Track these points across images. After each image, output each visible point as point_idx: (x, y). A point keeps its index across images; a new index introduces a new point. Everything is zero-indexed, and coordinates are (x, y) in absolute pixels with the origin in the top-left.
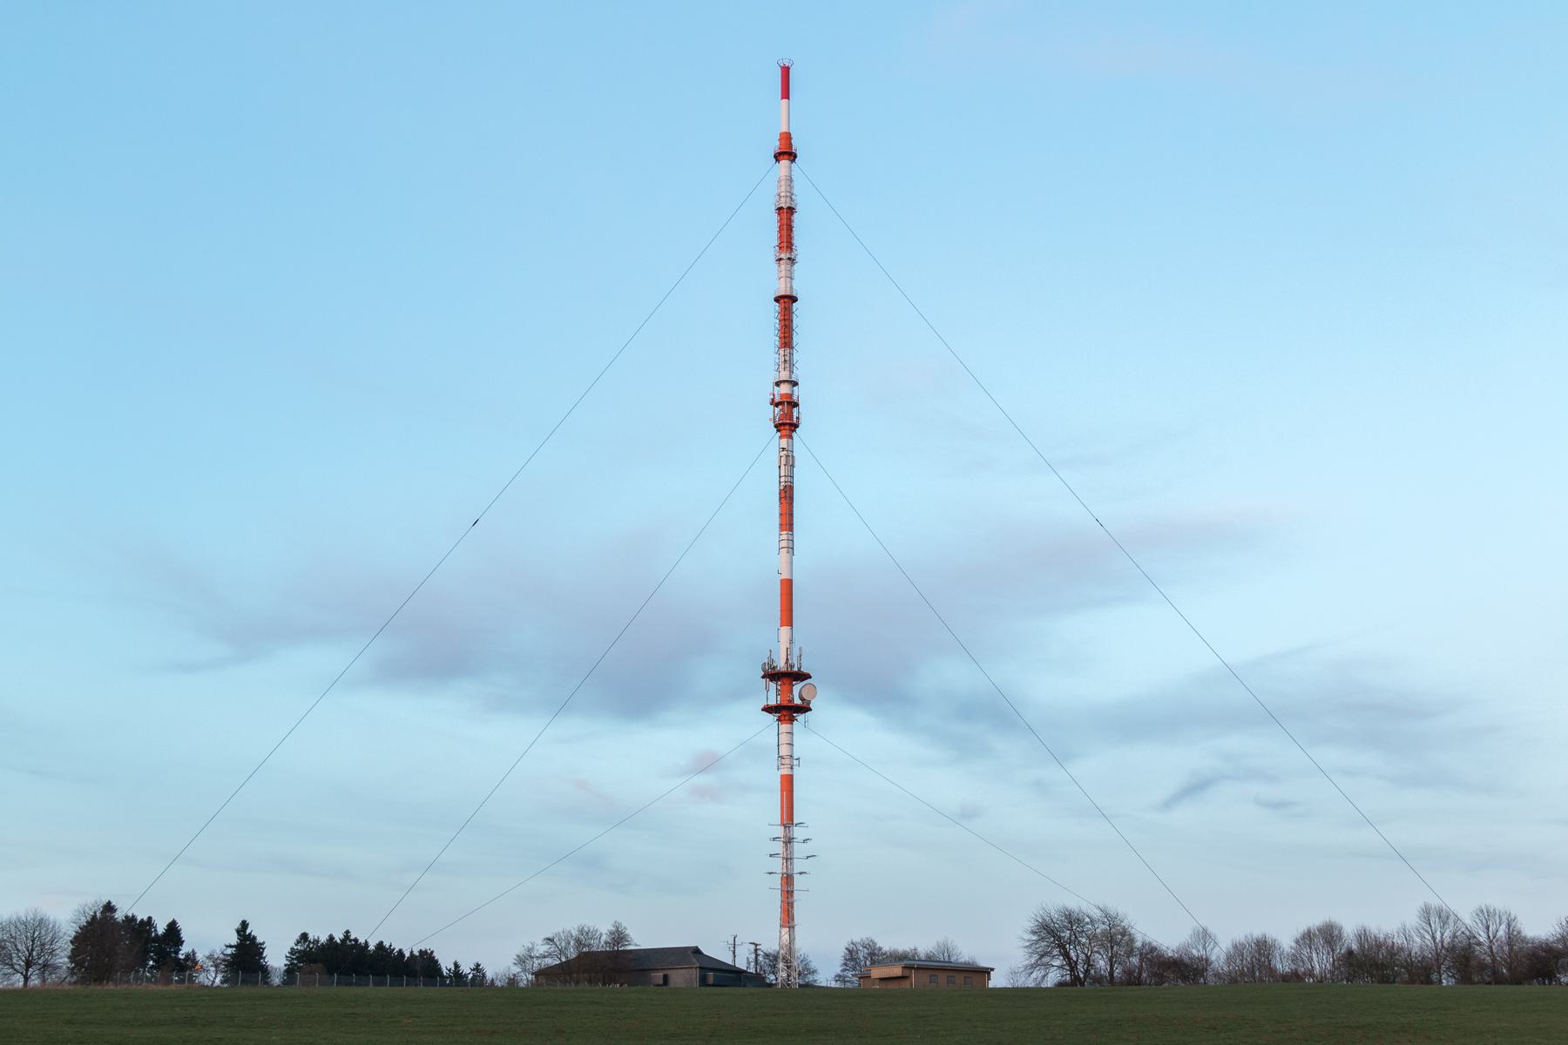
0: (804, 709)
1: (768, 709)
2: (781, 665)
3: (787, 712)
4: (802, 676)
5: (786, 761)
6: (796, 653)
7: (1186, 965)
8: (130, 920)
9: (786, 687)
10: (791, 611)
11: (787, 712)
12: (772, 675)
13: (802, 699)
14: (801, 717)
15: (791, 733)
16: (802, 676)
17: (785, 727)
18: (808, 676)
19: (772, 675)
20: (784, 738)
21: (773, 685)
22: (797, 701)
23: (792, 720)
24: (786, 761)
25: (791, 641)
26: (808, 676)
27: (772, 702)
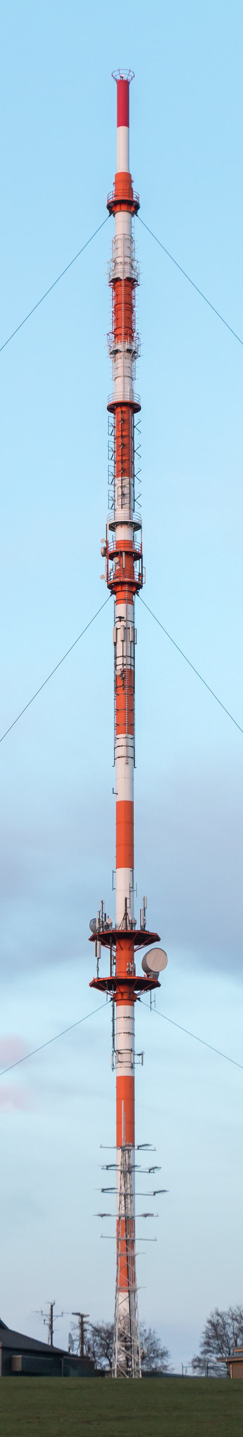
0: (150, 983)
1: (99, 984)
2: (117, 922)
4: (146, 938)
5: (125, 1057)
6: (138, 906)
9: (124, 953)
11: (125, 988)
12: (105, 937)
13: (147, 970)
14: (145, 996)
15: (131, 1018)
16: (146, 938)
17: (122, 1010)
19: (105, 937)
20: (121, 1025)
22: (140, 973)
23: (132, 1000)
24: (125, 1057)
25: (131, 889)
27: (105, 974)
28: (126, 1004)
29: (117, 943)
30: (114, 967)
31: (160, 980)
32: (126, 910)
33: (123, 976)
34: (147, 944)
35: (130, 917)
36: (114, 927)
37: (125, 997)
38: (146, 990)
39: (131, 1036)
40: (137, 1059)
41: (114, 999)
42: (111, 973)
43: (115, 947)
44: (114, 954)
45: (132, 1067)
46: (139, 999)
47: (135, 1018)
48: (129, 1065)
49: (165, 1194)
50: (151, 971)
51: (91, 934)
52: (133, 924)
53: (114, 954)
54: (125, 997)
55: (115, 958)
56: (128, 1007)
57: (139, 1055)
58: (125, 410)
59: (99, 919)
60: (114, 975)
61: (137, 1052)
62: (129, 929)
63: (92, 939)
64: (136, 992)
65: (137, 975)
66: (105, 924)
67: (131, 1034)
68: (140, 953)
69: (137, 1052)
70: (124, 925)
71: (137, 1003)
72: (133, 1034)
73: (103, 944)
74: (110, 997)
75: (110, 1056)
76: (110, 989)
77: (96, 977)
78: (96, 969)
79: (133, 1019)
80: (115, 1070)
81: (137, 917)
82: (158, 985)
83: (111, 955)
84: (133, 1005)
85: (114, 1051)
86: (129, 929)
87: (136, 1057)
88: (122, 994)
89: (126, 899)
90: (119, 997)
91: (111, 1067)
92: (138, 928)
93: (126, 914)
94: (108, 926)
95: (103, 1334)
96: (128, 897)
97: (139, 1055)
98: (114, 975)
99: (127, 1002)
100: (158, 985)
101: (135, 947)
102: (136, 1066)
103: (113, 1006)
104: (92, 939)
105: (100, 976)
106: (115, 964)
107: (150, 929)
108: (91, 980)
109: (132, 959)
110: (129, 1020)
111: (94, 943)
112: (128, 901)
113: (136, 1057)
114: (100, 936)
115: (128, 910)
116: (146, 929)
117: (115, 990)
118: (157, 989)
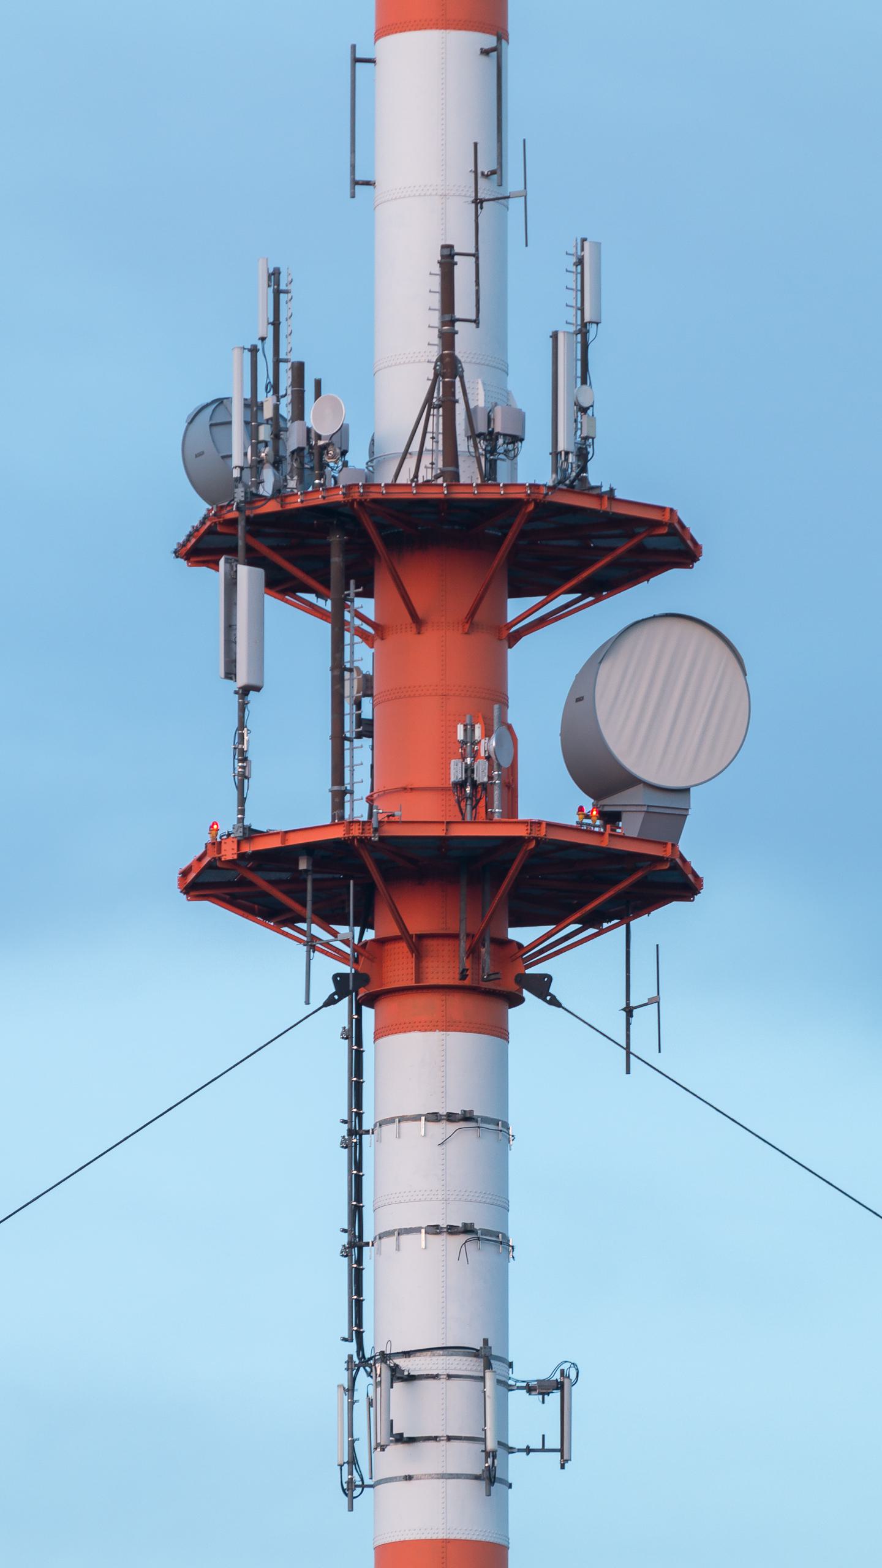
0: (618, 875)
1: (253, 880)
2: (380, 422)
3: (446, 904)
4: (589, 545)
5: (439, 1406)
6: (534, 304)
7: (210, 531)
8: (521, 1000)
9: (438, 654)
10: (599, 258)
11: (446, 904)
12: (298, 532)
13: (599, 774)
14: (586, 967)
15: (481, 1122)
16: (589, 545)
17: (418, 1063)
18: (650, 545)
19: (298, 532)
20: (413, 1174)
21: (294, 637)
22: (551, 799)
23: (493, 989)
24: (439, 1406)
25: (489, 184)
26: (650, 545)
27: (294, 802)
28: (448, 1026)
29: (383, 581)
30: (361, 753)
31: (692, 847)
32: (447, 339)
33: (424, 816)
34: (599, 587)
35: (477, 392)
36: (357, 458)
37: (442, 969)
38: (595, 920)
39: (481, 1255)
40: (529, 1419)
41: (358, 988)
42: (339, 797)
43: (367, 606)
44: (362, 656)
45: (491, 1477)
46: (541, 987)
47: (519, 1117)
48: (467, 1459)
49: (294, 276)
50: (632, 781)
51: (195, 510)
52: (497, 441)
53: (362, 656)
54: (442, 969)
55: (367, 686)
56: (462, 1045)
57: (540, 1389)
58: (449, 1377)
59: (253, 406)
60: (359, 810)
61: (529, 1361)
62: (469, 473)
63: (201, 549)
64: (523, 935)
65: (525, 813)
66: (294, 439)
67: (483, 1237)
68: (549, 658)
69: (529, 1361)
70: (434, 445)
71: (526, 1017)
72: (499, 1240)
73: (280, 584)
74: (327, 968)
75: (335, 1401)
76: (330, 916)
77: (228, 824)
78: (227, 765)
79: (500, 1127)
80: (365, 1500)
81: (528, 389)
82: (684, 885)
83: (339, 669)
84: (502, 1033)
85: (359, 1363)
86: (469, 473)
87: (518, 1400)
88: (418, 944)
89: (448, 259)
90: (399, 968)
91: (333, 1478)
92: (532, 468)
93: (448, 368)
94: (316, 455)
95: (468, 761)
96: (463, 243)
97: (540, 1389)
98: (359, 810)
99: (458, 1004)
100: (678, 884)
101: (516, 607)
102: (516, 1467)
103: (354, 1035)
104: (201, 549)
105: (256, 820)
106: (366, 729)
107: (623, 473)
108: (190, 849)
109: (490, 698)
110: (465, 1139)
111: (212, 579)
112: (463, 270)
113: (518, 1400)
114: (258, 525)
115: (464, 334)
116: (596, 476)
117: (366, 923)
118: (674, 909)
